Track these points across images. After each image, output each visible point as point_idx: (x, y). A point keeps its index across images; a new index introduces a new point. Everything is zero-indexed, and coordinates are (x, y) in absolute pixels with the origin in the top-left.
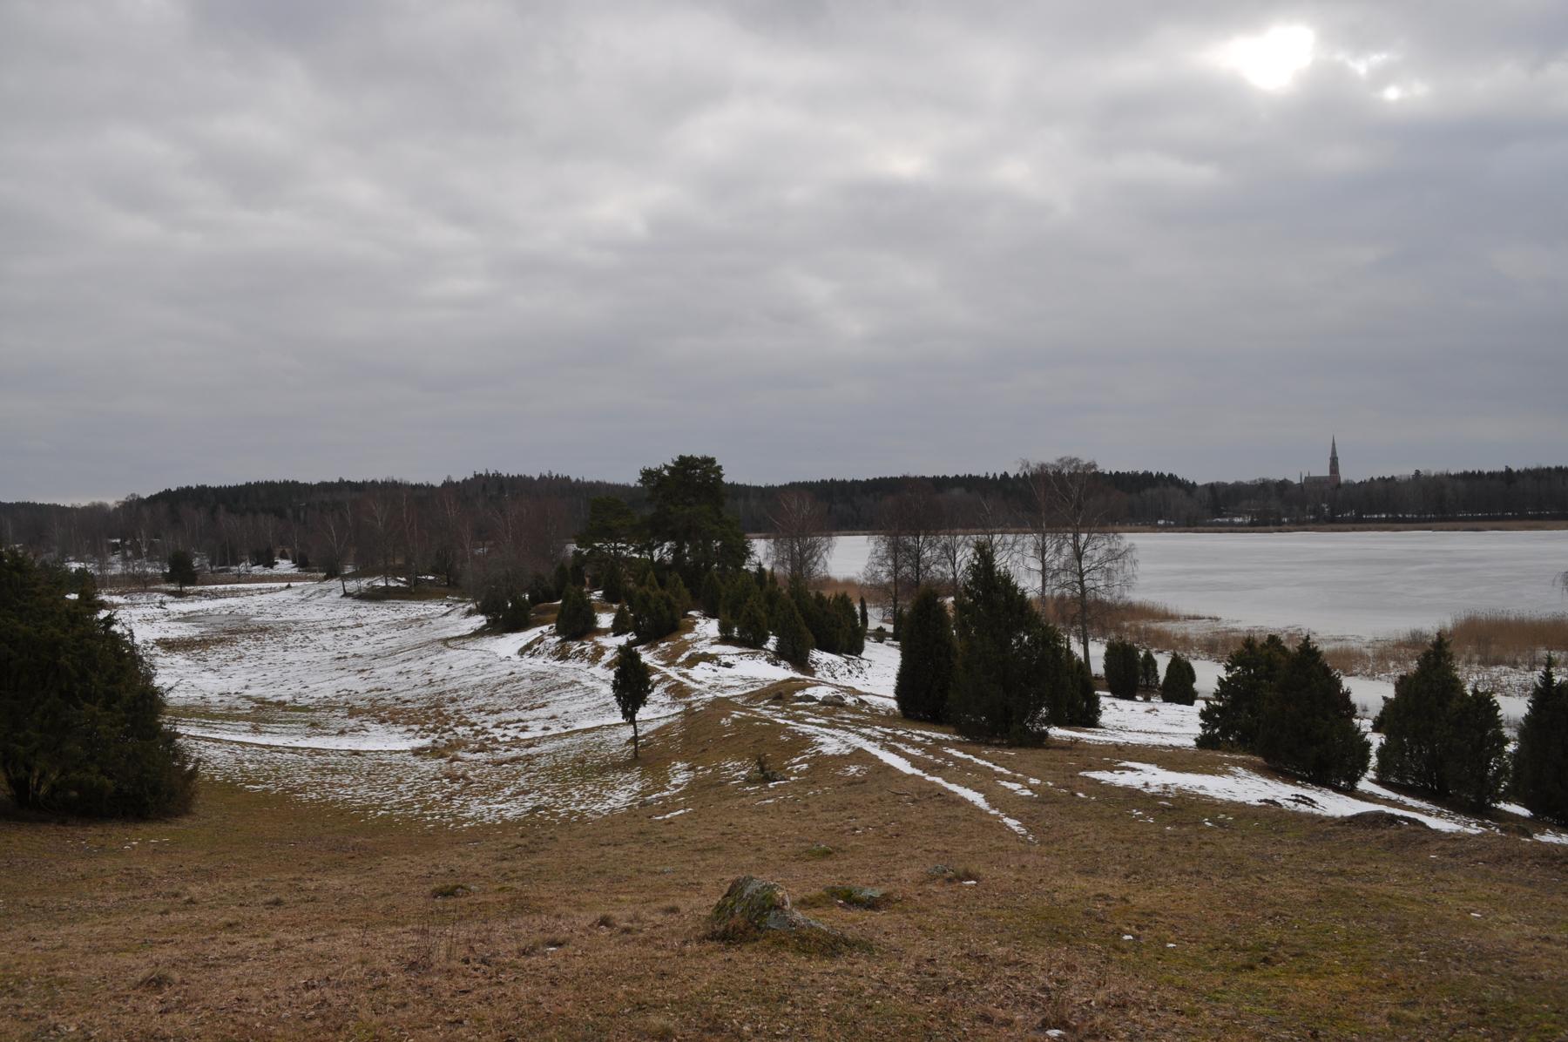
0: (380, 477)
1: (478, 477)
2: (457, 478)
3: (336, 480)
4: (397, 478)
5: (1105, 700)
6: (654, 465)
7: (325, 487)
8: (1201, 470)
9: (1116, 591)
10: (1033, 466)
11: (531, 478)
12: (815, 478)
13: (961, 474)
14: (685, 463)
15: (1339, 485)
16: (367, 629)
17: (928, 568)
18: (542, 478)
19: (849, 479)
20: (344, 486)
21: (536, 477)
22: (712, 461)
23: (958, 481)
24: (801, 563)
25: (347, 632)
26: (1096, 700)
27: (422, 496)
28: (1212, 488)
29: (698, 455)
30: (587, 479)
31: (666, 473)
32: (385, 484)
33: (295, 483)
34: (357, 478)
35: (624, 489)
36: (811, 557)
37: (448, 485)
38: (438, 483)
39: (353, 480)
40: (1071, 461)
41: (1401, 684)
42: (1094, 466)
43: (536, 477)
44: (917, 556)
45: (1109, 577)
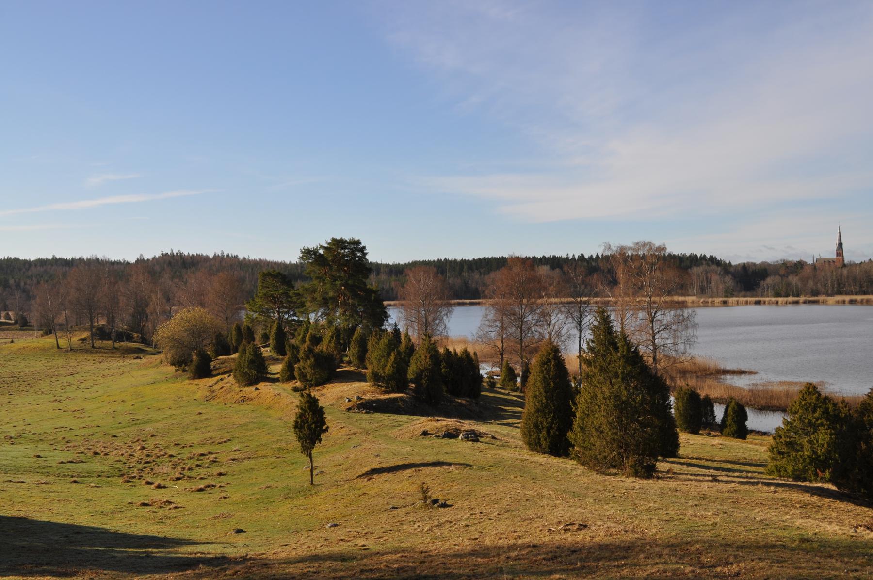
0: (86, 255)
1: (164, 255)
2: (148, 256)
3: (50, 257)
4: (100, 256)
5: (684, 437)
6: (312, 246)
7: (41, 262)
8: (738, 248)
9: (681, 347)
10: (614, 248)
11: (207, 257)
12: (432, 257)
13: (547, 255)
14: (338, 243)
15: (844, 265)
16: (78, 377)
17: (529, 329)
18: (216, 257)
19: (459, 259)
20: (57, 262)
21: (211, 256)
22: (358, 243)
23: (544, 261)
24: (427, 327)
25: (61, 379)
26: (676, 437)
27: (27, 264)
28: (745, 267)
29: (347, 238)
30: (252, 258)
31: (321, 252)
32: (89, 260)
33: (17, 260)
34: (67, 255)
35: (291, 266)
36: (434, 319)
37: (141, 262)
38: (133, 260)
39: (64, 257)
40: (644, 245)
41: (482, 377)
42: (664, 249)
43: (211, 256)
44: (521, 322)
45: (675, 337)
